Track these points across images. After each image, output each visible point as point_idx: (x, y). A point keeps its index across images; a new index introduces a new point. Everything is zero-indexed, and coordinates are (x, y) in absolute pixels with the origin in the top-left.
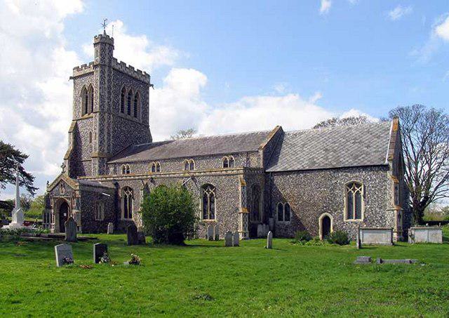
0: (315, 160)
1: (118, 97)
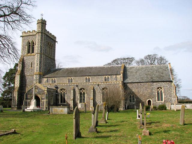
0: (143, 78)
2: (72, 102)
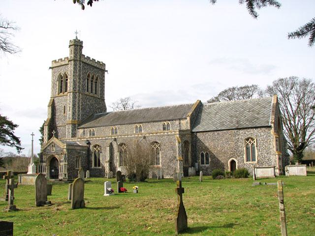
1: (84, 78)
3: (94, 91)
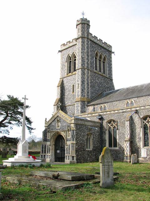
2: (128, 145)
3: (102, 71)
